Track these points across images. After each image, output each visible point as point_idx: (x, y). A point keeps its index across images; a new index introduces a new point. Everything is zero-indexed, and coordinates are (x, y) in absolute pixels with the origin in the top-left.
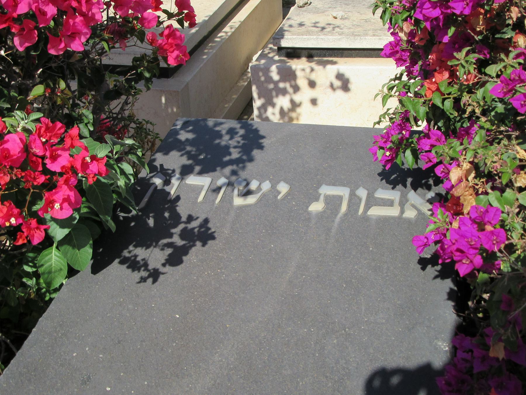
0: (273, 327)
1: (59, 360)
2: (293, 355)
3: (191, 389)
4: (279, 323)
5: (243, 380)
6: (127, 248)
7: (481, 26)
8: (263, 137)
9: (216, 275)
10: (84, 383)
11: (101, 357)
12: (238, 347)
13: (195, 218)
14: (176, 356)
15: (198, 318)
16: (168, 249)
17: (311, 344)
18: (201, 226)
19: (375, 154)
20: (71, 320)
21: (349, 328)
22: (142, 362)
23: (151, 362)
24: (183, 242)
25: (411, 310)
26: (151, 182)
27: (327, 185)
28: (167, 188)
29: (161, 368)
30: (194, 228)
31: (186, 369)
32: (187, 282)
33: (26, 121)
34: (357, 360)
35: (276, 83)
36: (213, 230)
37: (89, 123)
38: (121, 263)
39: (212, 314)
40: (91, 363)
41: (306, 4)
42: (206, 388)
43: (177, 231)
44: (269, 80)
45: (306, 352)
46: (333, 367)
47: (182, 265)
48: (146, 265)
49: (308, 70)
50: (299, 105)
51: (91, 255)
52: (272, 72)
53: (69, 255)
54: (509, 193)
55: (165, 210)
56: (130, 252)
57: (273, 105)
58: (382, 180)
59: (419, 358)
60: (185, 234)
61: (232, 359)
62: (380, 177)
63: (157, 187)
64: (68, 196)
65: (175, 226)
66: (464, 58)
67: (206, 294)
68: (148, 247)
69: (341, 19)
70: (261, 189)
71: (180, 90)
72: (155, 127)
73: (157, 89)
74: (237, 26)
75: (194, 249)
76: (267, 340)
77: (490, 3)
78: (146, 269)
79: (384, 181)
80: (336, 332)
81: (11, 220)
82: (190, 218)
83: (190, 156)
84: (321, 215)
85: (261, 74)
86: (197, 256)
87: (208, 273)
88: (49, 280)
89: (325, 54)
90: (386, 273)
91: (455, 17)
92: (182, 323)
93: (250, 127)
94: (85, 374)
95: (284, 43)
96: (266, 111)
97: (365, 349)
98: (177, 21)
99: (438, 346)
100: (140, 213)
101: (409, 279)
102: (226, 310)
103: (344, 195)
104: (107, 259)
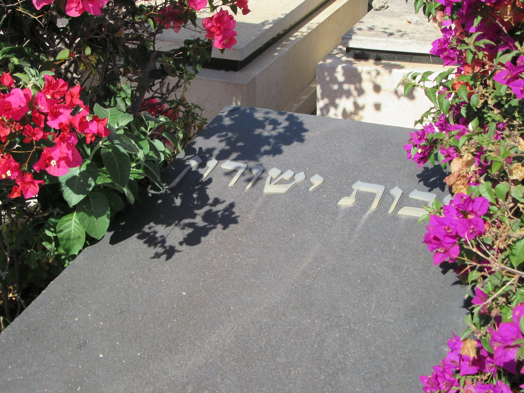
0: (277, 315)
1: (60, 323)
2: (291, 344)
3: (181, 365)
4: (284, 311)
5: (236, 362)
6: (148, 223)
7: (509, 16)
8: (306, 130)
9: (231, 258)
10: (80, 347)
11: (101, 325)
12: (237, 330)
13: (221, 201)
14: (174, 332)
15: (203, 297)
16: (189, 229)
17: (312, 335)
18: (226, 210)
19: (409, 151)
20: (80, 286)
21: (354, 324)
22: (140, 334)
23: (149, 335)
24: (205, 224)
25: (423, 313)
26: (187, 163)
27: (362, 182)
28: (201, 171)
29: (157, 341)
30: (218, 211)
31: (181, 346)
32: (200, 263)
33: (37, 79)
34: (356, 356)
35: (341, 84)
36: (237, 214)
37: (126, 97)
38: (139, 237)
39: (219, 295)
40: (90, 329)
41: (383, 7)
42: (197, 366)
43: (201, 212)
44: (334, 80)
45: (305, 342)
46: (329, 360)
47: (200, 245)
48: (163, 241)
49: (374, 73)
50: (362, 108)
51: (109, 225)
52: (337, 72)
53: (86, 222)
54: (503, 186)
55: (194, 191)
56: (150, 228)
57: (336, 106)
58: (420, 181)
59: (421, 362)
60: (210, 217)
61: (229, 341)
62: (419, 178)
63: (191, 168)
64: (67, 154)
65: (200, 207)
66: (474, 43)
67: (217, 276)
68: (169, 225)
69: (415, 24)
70: (294, 180)
71: (245, 84)
72: (203, 112)
73: (224, 81)
74: (314, 27)
75: (214, 231)
76: (268, 326)
78: (163, 246)
79: (422, 183)
80: (341, 326)
81: (7, 173)
82: (217, 201)
83: (229, 142)
84: (350, 211)
85: (326, 74)
86: (216, 238)
87: (224, 256)
88: (67, 246)
89: (394, 58)
90: (405, 273)
91: (483, 7)
92: (187, 300)
93: (295, 120)
94: (82, 339)
95: (352, 44)
96: (328, 111)
97: (367, 346)
98: (230, 6)
99: (444, 352)
100: (169, 192)
101: (428, 281)
102: (233, 293)
103: (378, 192)
104: (128, 232)
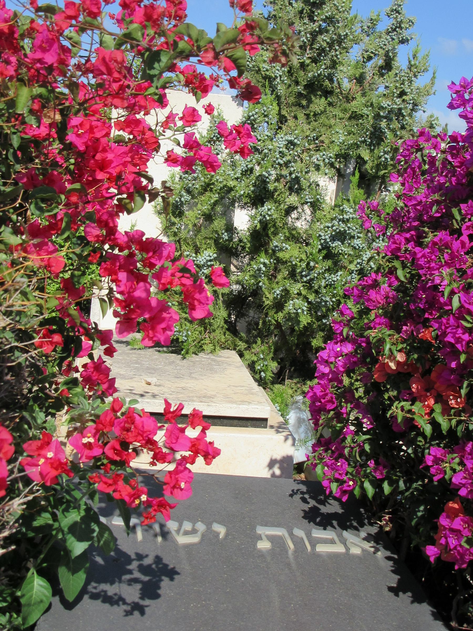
77: (319, 404)
